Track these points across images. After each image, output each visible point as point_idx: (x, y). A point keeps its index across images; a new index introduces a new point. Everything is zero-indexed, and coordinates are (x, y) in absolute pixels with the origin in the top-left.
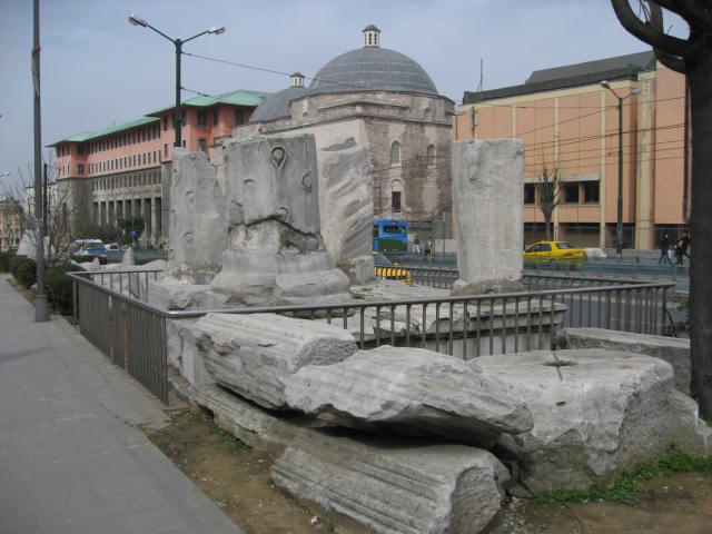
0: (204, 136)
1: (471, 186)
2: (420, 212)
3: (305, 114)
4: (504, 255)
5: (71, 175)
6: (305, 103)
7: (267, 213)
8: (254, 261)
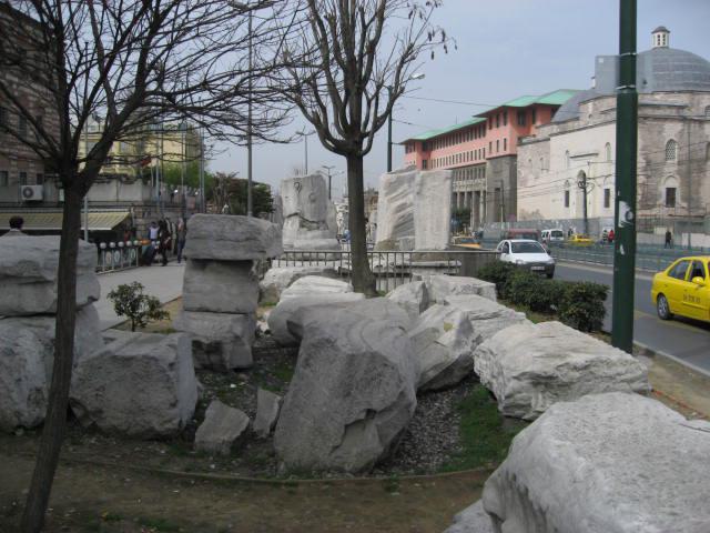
2: (698, 208)
6: (590, 105)
7: (293, 212)
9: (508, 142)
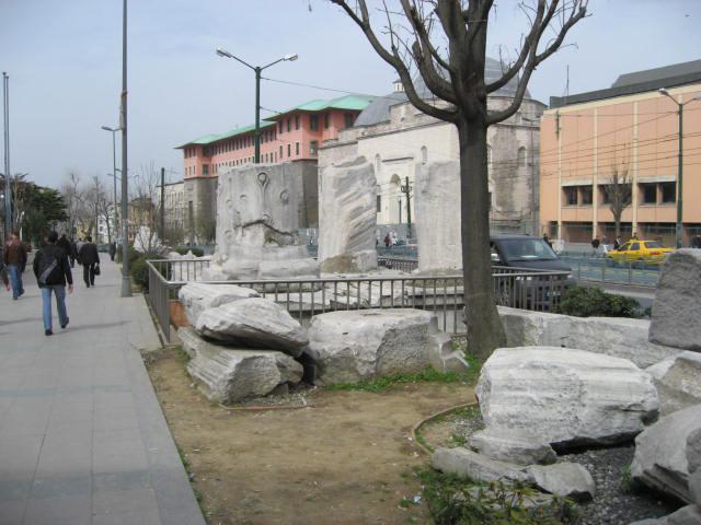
0: (206, 163)
1: (423, 198)
2: (512, 212)
3: (403, 119)
4: (450, 250)
5: (196, 176)
7: (255, 218)
8: (246, 252)
9: (300, 146)
